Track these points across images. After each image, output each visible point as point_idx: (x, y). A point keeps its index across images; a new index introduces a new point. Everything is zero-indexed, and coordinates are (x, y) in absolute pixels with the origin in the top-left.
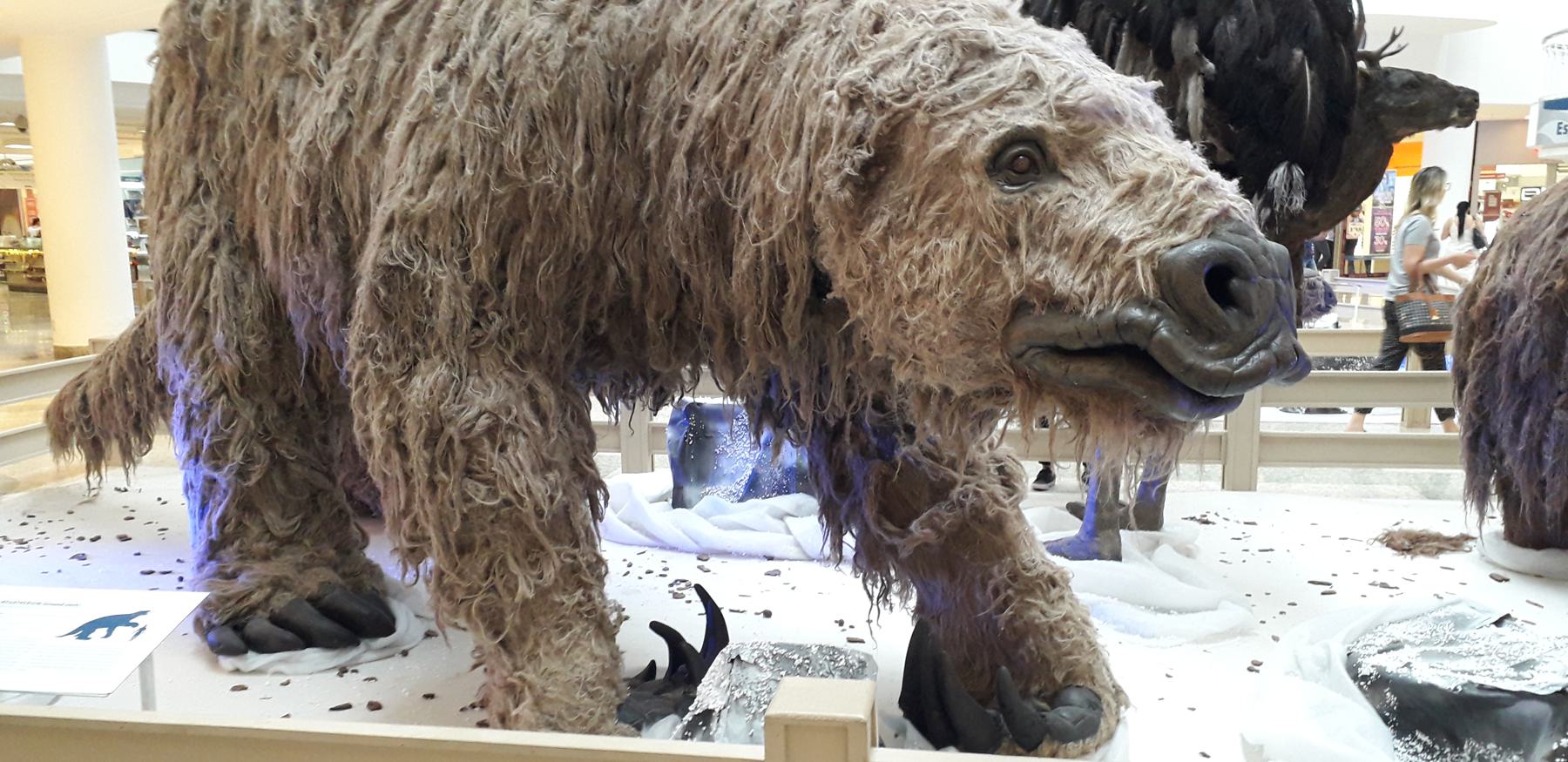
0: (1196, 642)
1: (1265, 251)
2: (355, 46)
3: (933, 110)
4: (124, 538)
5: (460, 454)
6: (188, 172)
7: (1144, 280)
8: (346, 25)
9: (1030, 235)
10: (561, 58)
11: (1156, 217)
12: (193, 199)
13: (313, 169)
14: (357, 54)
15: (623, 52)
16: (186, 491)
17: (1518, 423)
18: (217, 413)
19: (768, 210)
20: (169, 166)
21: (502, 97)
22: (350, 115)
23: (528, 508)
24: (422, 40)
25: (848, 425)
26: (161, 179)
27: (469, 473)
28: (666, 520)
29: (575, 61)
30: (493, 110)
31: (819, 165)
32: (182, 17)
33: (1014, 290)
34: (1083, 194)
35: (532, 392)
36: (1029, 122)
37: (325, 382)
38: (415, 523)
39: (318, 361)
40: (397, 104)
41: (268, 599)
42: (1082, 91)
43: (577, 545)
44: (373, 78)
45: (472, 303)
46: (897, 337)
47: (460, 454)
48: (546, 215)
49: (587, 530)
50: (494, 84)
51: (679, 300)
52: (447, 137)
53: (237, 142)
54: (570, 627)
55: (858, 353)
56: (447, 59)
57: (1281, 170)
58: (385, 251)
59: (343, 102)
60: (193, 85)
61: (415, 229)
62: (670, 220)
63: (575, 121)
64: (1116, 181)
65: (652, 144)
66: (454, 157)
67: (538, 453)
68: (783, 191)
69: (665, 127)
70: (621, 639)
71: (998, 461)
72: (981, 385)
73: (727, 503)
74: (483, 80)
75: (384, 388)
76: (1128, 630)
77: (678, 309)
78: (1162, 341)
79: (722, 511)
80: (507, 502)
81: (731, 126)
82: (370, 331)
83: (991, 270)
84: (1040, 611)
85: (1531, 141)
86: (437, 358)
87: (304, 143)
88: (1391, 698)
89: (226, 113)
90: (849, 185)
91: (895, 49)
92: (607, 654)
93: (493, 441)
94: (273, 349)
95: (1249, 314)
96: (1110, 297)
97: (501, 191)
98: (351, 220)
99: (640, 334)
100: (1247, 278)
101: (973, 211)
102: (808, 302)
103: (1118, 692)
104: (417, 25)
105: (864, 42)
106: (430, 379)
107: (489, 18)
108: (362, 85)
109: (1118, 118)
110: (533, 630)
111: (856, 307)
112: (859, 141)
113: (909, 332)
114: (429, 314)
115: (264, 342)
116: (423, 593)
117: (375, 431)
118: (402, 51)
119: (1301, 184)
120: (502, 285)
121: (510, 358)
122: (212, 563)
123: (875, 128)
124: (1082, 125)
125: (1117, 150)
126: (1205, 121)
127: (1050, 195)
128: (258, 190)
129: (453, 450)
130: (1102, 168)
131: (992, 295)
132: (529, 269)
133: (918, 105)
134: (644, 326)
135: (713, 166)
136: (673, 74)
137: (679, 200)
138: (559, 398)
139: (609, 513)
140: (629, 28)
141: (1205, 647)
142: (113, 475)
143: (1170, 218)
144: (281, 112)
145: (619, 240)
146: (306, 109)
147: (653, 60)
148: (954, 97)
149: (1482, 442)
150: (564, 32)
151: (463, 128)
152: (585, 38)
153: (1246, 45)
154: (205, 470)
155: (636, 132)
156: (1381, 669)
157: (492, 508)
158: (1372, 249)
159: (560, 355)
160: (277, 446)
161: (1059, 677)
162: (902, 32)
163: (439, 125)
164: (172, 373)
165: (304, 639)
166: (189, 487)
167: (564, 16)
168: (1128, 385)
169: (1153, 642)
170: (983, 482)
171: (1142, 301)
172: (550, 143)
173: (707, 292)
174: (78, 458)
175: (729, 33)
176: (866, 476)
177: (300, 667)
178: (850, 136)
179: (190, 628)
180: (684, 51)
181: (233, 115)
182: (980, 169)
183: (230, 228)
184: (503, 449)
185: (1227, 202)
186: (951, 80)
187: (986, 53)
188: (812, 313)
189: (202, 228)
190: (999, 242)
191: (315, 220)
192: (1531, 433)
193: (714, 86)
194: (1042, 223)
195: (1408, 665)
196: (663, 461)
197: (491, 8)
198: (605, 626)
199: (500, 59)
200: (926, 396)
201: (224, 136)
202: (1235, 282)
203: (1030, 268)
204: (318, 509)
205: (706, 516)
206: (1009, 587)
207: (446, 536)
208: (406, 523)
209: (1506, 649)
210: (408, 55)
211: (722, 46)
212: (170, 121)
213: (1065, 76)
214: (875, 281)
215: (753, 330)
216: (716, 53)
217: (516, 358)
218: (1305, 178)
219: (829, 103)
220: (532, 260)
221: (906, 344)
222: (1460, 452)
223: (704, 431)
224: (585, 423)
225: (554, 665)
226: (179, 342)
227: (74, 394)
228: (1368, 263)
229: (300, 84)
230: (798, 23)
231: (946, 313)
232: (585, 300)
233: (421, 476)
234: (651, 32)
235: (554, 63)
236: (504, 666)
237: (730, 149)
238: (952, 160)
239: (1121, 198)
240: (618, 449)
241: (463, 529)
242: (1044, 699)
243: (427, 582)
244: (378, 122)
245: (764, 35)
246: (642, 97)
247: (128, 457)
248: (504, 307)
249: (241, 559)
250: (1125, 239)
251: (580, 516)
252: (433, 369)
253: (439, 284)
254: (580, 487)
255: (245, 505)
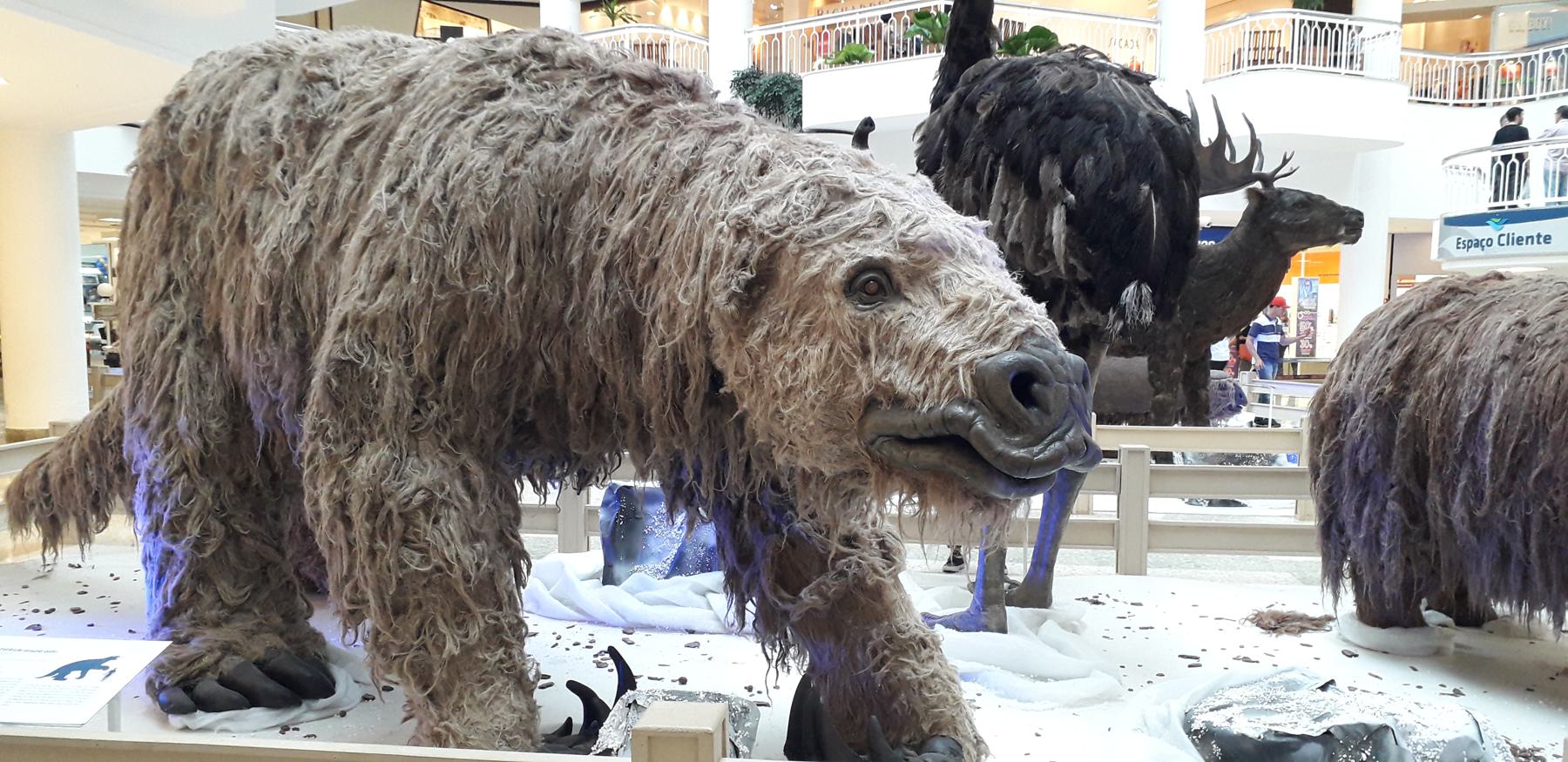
0: (1070, 706)
1: (1062, 362)
2: (318, 166)
3: (802, 242)
4: (77, 611)
5: (398, 525)
6: (161, 272)
7: (964, 383)
8: (310, 146)
9: (879, 345)
10: (497, 186)
11: (976, 333)
12: (164, 296)
13: (276, 272)
14: (319, 172)
15: (552, 181)
16: (144, 562)
17: (1359, 512)
18: (177, 491)
19: (673, 318)
20: (143, 265)
21: (445, 218)
22: (311, 225)
23: (457, 574)
24: (377, 164)
25: (747, 502)
26: (135, 276)
27: (405, 542)
28: (597, 597)
29: (510, 189)
30: (437, 228)
31: (713, 282)
32: (161, 135)
33: (866, 390)
34: (920, 313)
35: (464, 471)
36: (878, 254)
37: (279, 463)
38: (356, 588)
39: (273, 444)
40: (353, 218)
41: (217, 662)
42: (922, 229)
43: (500, 609)
44: (333, 194)
45: (413, 393)
46: (776, 426)
47: (398, 525)
48: (481, 318)
49: (511, 595)
50: (438, 206)
51: (598, 392)
52: (396, 250)
53: (207, 245)
54: (492, 682)
55: (748, 439)
56: (398, 183)
57: (1132, 288)
58: (338, 347)
59: (305, 214)
60: (168, 194)
61: (365, 329)
62: (589, 324)
63: (508, 240)
64: (946, 303)
65: (575, 260)
66: (402, 267)
67: (467, 526)
68: (684, 302)
69: (587, 245)
70: (538, 695)
71: (878, 536)
72: (846, 468)
73: (653, 580)
74: (429, 203)
75: (333, 467)
76: (1007, 695)
77: (597, 400)
78: (979, 434)
79: (648, 588)
80: (438, 569)
81: (642, 247)
82: (322, 416)
83: (848, 373)
84: (914, 669)
85: (1434, 255)
86: (380, 440)
87: (268, 250)
88: (1217, 750)
89: (198, 220)
90: (735, 300)
91: (775, 190)
92: (524, 707)
93: (428, 515)
94: (233, 433)
95: (1047, 412)
96: (939, 397)
97: (442, 297)
98: (309, 318)
99: (564, 419)
100: (1046, 383)
101: (834, 324)
102: (706, 395)
103: (979, 742)
104: (374, 150)
105: (751, 183)
106: (374, 459)
107: (436, 149)
108: (323, 200)
109: (950, 252)
110: (458, 685)
111: (742, 400)
112: (744, 264)
113: (784, 422)
114: (375, 402)
115: (224, 426)
116: (360, 652)
117: (324, 504)
118: (360, 171)
119: (1149, 301)
120: (441, 378)
121: (445, 441)
122: (167, 629)
123: (757, 253)
124: (920, 257)
125: (948, 277)
126: (1067, 242)
127: (894, 313)
128: (225, 288)
129: (392, 522)
130: (936, 292)
131: (849, 393)
132: (465, 364)
133: (790, 237)
134: (567, 415)
135: (627, 281)
136: (595, 202)
137: (597, 307)
138: (488, 477)
139: (532, 582)
140: (556, 162)
141: (1075, 710)
142: (69, 552)
143: (986, 334)
144: (248, 221)
145: (546, 340)
146: (272, 219)
147: (578, 189)
148: (819, 231)
149: (1334, 530)
150: (500, 163)
151: (411, 243)
152: (519, 169)
153: (1101, 179)
154: (164, 542)
155: (563, 248)
156: (1208, 724)
157: (425, 574)
158: (1298, 353)
159: (491, 439)
160: (232, 521)
161: (926, 727)
162: (781, 175)
163: (390, 240)
164: (137, 453)
165: (251, 699)
166: (147, 559)
167: (501, 150)
168: (953, 468)
169: (1028, 705)
170: (865, 554)
171: (963, 401)
172: (487, 257)
173: (621, 385)
174: (35, 535)
175: (642, 168)
176: (765, 549)
177: (246, 725)
178: (737, 260)
179: (141, 689)
180: (603, 183)
181: (204, 222)
182: (839, 292)
183: (198, 322)
184: (436, 521)
185: (1032, 322)
186: (818, 217)
187: (848, 196)
188: (711, 405)
189: (172, 322)
190: (854, 350)
191: (276, 317)
192: (1370, 522)
193: (628, 213)
194: (888, 335)
195: (1230, 720)
196: (596, 541)
197: (439, 140)
198: (524, 682)
199: (445, 186)
200: (806, 477)
201: (196, 240)
202: (1036, 386)
203: (878, 372)
204: (268, 580)
205: (632, 592)
206: (885, 647)
207: (383, 599)
208: (348, 587)
209: (1313, 706)
210: (365, 176)
211: (636, 180)
212: (145, 224)
213: (908, 217)
214: (757, 379)
215: (659, 419)
216: (631, 185)
217: (451, 442)
218: (1153, 295)
219: (721, 231)
220: (468, 356)
221: (783, 432)
222: (1315, 540)
223: (635, 512)
224: (512, 500)
225: (476, 716)
226: (145, 425)
227: (35, 474)
228: (1294, 365)
229: (267, 196)
230: (700, 162)
231: (813, 406)
232: (515, 390)
233: (362, 544)
234: (576, 165)
235: (490, 190)
236: (431, 716)
237: (641, 266)
238: (816, 283)
239: (950, 317)
240: (555, 530)
241: (398, 593)
242: (913, 748)
243: (365, 641)
244: (336, 231)
245: (671, 172)
246: (568, 219)
247: (84, 534)
248: (442, 396)
249: (194, 625)
250: (951, 350)
251: (504, 582)
252: (377, 450)
253: (385, 376)
254: (505, 556)
255: (200, 575)
